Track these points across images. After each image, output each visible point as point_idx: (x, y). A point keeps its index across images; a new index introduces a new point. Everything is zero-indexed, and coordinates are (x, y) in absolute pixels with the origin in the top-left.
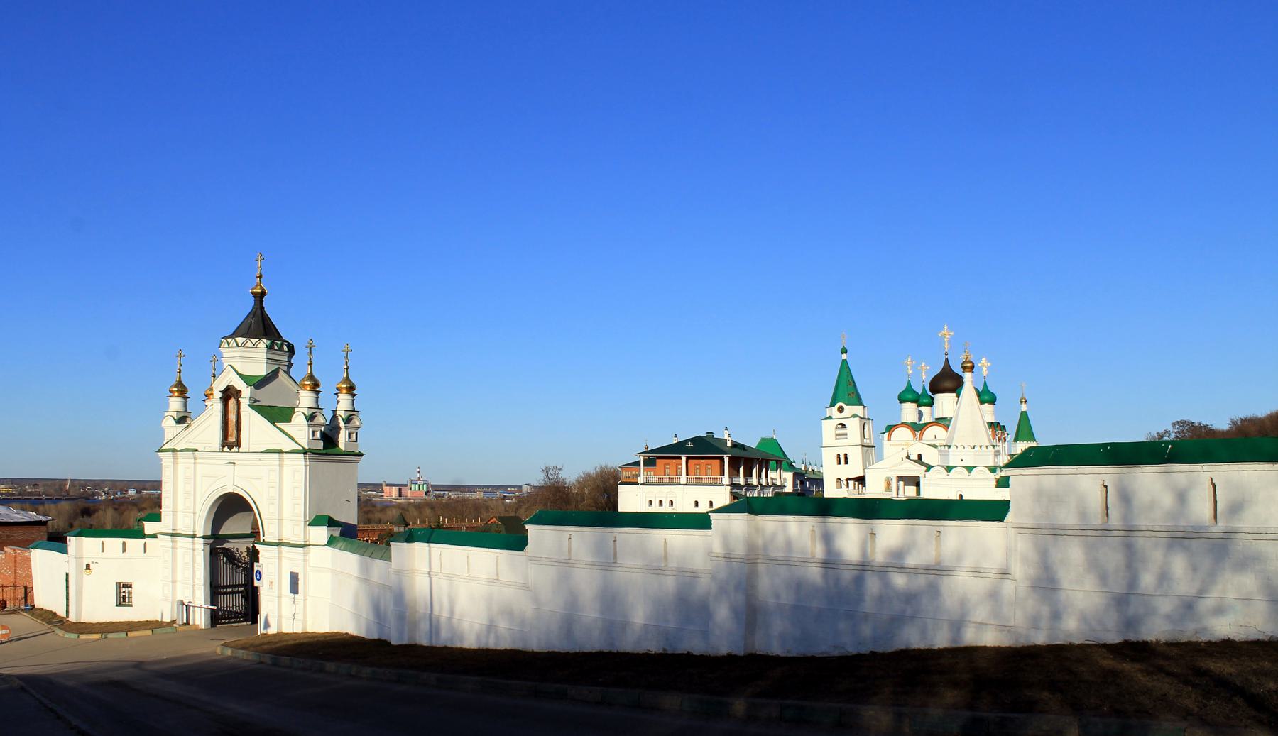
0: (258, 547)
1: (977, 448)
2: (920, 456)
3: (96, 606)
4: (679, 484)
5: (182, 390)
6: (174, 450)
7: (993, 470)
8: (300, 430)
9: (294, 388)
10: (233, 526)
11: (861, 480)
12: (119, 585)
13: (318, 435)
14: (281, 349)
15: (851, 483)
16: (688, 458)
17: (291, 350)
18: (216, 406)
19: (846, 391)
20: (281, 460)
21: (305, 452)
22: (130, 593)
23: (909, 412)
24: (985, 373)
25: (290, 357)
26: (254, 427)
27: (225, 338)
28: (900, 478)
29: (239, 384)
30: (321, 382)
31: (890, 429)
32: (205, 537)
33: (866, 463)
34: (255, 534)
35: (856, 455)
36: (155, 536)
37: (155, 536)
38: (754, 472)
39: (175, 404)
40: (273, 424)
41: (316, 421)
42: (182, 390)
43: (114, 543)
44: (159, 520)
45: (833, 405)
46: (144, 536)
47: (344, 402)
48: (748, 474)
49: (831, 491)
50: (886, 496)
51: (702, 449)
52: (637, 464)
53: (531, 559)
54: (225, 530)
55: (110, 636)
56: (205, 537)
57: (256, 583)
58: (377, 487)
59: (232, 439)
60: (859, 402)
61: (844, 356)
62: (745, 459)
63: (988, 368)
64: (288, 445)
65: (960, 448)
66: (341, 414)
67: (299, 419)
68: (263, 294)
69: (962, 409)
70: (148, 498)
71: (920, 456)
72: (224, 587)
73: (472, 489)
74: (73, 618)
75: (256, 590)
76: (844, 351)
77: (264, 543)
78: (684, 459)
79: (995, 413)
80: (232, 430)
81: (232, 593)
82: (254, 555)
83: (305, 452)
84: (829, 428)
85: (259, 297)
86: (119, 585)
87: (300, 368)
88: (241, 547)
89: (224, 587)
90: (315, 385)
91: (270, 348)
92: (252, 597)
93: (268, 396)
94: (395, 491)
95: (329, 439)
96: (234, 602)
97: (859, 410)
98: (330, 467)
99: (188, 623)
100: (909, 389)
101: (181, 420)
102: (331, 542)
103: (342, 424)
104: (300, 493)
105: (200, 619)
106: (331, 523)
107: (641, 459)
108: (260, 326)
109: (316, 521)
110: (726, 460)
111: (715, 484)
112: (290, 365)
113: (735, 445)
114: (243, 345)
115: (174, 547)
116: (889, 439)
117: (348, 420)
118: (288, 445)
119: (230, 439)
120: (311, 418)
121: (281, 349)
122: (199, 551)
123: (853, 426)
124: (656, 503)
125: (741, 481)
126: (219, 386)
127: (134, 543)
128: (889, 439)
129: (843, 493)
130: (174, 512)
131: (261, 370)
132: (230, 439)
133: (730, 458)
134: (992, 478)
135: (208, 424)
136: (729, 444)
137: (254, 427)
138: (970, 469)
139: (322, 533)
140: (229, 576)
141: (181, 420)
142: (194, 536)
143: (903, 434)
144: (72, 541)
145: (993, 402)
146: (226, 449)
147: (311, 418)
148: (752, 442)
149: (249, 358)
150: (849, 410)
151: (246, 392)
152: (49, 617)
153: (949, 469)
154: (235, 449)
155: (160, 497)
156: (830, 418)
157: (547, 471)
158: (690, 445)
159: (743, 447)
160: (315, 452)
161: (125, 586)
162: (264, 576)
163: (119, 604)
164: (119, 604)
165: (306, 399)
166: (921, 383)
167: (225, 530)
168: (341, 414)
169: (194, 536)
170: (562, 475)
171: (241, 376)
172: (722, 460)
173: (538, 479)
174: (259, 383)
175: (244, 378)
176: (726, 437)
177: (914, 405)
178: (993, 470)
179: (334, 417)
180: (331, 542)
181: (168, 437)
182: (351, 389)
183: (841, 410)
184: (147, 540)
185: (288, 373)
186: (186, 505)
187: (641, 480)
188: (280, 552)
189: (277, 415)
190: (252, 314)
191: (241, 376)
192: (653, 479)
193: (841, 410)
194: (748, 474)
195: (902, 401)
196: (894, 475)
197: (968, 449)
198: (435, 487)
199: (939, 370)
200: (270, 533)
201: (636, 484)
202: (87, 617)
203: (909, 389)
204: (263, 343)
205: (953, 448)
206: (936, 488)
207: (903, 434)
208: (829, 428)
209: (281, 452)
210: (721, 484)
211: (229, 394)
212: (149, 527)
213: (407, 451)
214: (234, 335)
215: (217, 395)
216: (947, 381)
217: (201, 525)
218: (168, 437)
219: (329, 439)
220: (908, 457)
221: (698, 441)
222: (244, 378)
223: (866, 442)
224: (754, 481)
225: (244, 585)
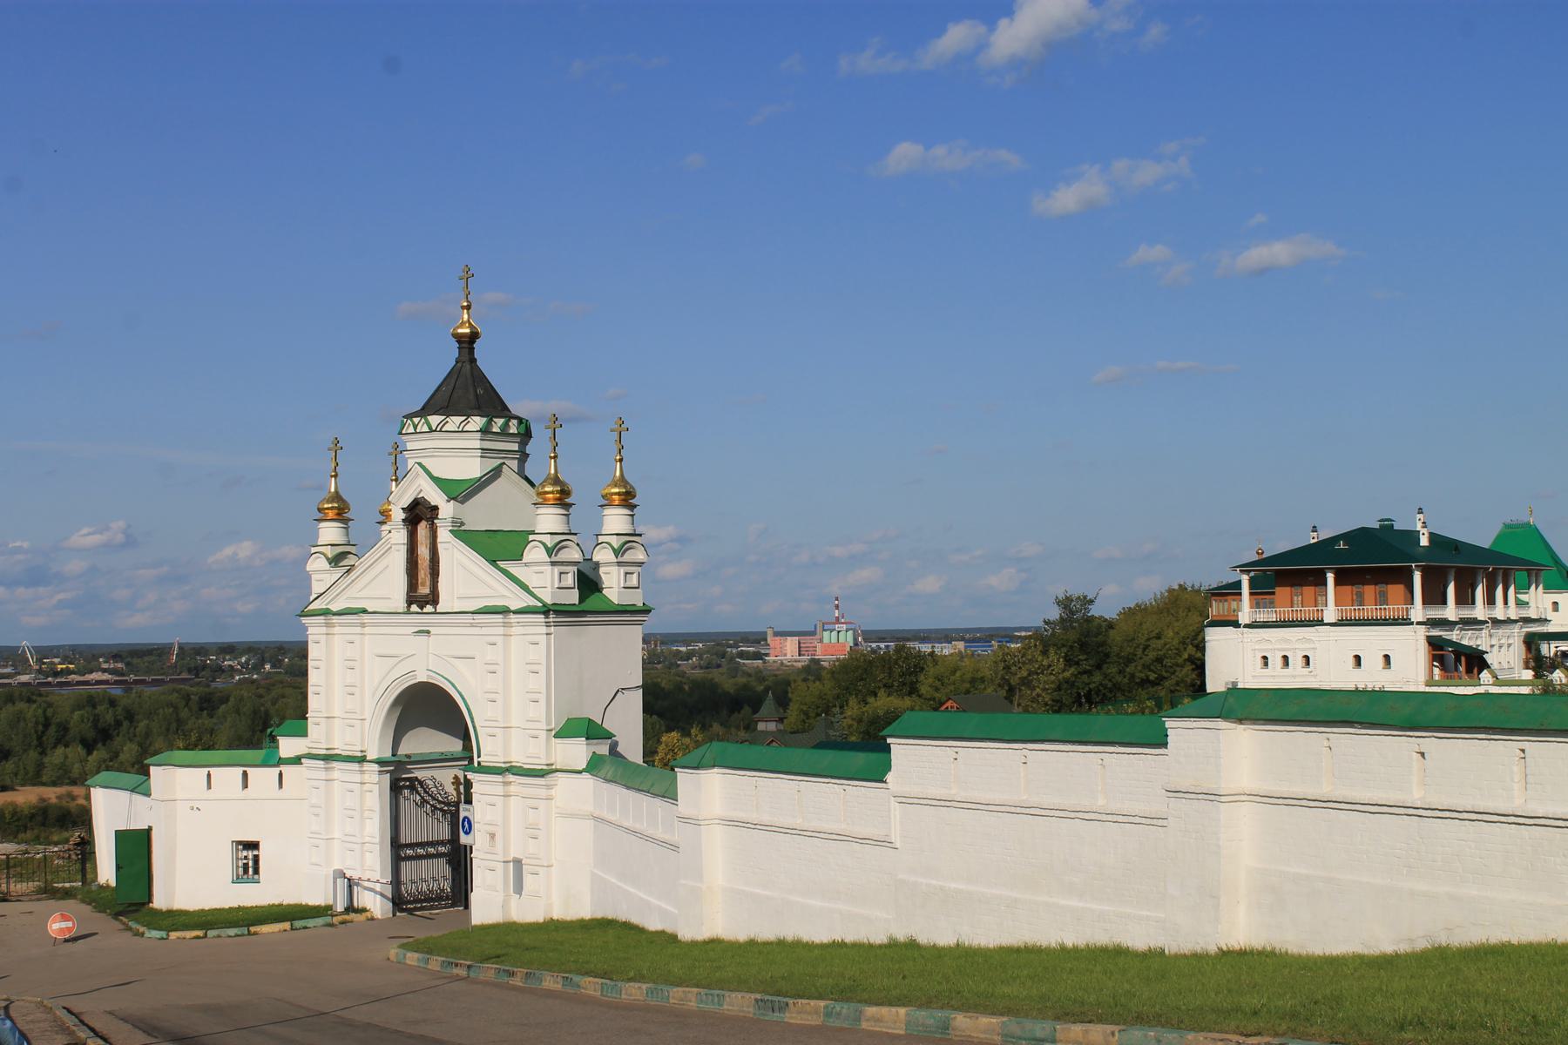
0: (470, 776)
4: (1320, 623)
6: (326, 613)
18: (397, 536)
21: (546, 611)
22: (256, 859)
25: (523, 444)
29: (435, 496)
30: (572, 485)
34: (467, 755)
36: (297, 760)
37: (297, 760)
38: (1480, 592)
40: (493, 562)
44: (147, 834)
46: (281, 762)
48: (1465, 599)
53: (905, 800)
57: (464, 839)
59: (424, 590)
67: (535, 553)
68: (474, 336)
81: (429, 856)
83: (546, 611)
85: (468, 343)
88: (445, 778)
89: (411, 846)
92: (460, 860)
93: (484, 513)
96: (431, 874)
101: (336, 561)
104: (538, 683)
105: (375, 903)
107: (1245, 579)
108: (467, 392)
109: (566, 731)
110: (1417, 577)
112: (523, 457)
118: (518, 600)
119: (422, 593)
121: (504, 433)
122: (372, 789)
124: (1275, 661)
125: (1451, 611)
126: (401, 498)
127: (263, 777)
130: (472, 625)
131: (470, 468)
132: (422, 593)
135: (383, 575)
136: (1424, 541)
139: (577, 751)
141: (336, 561)
146: (414, 608)
148: (1481, 536)
149: (452, 451)
154: (429, 608)
157: (1065, 603)
162: (476, 826)
163: (237, 880)
165: (549, 520)
167: (403, 750)
169: (362, 760)
170: (1095, 611)
171: (438, 481)
173: (1040, 612)
189: (500, 547)
191: (438, 481)
194: (1465, 599)
200: (489, 750)
201: (1236, 624)
209: (505, 611)
210: (1406, 622)
211: (419, 513)
214: (425, 411)
215: (398, 515)
217: (373, 740)
218: (317, 588)
221: (1359, 538)
224: (1479, 611)
225: (449, 841)
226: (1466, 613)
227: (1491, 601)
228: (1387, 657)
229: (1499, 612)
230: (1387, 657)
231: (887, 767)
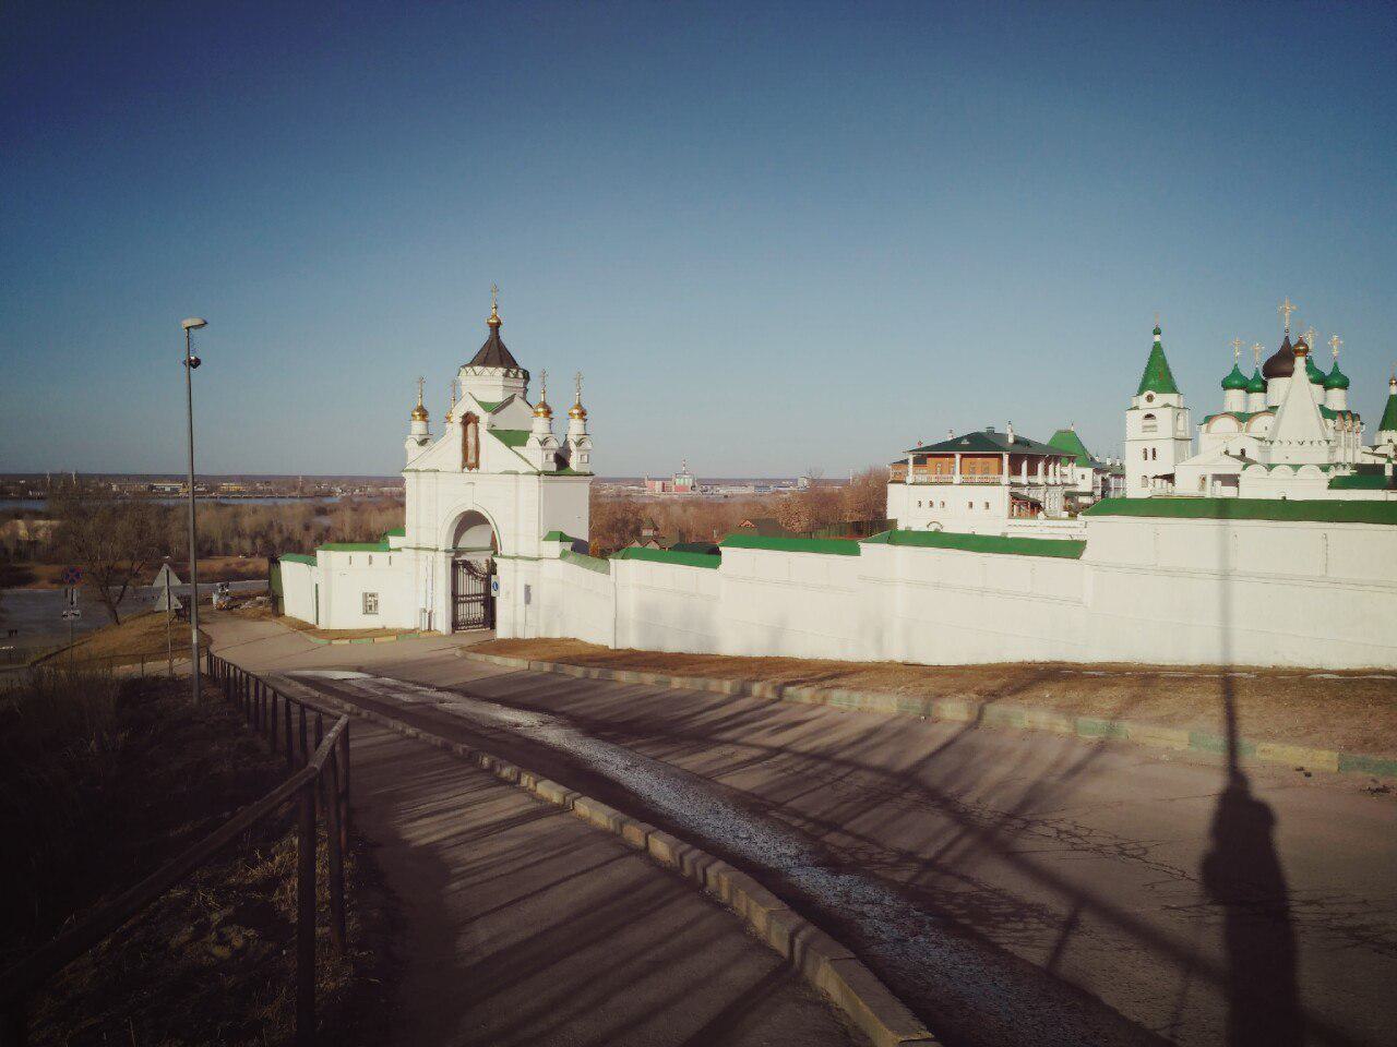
0: (496, 560)
1: (1307, 444)
2: (1243, 452)
3: (343, 614)
5: (424, 414)
6: (417, 471)
7: (1325, 468)
8: (536, 456)
9: (530, 412)
10: (474, 538)
11: (1170, 478)
12: (365, 595)
13: (552, 458)
14: (516, 376)
15: (1158, 481)
16: (963, 456)
17: (527, 376)
18: (455, 430)
19: (1158, 376)
20: (517, 481)
23: (1235, 400)
24: (1335, 353)
25: (526, 383)
26: (493, 451)
27: (464, 367)
28: (1216, 477)
29: (478, 411)
31: (1209, 419)
32: (447, 551)
33: (1179, 458)
35: (1166, 450)
36: (399, 550)
37: (399, 550)
38: (1041, 466)
39: (418, 427)
41: (548, 445)
42: (424, 414)
43: (360, 557)
45: (1141, 392)
47: (575, 427)
48: (1032, 471)
49: (1134, 488)
50: (1201, 494)
51: (981, 446)
52: (905, 462)
54: (461, 545)
55: (334, 642)
56: (447, 551)
57: (493, 593)
58: (639, 482)
59: (472, 460)
60: (1174, 390)
61: (1157, 338)
62: (1026, 455)
63: (1340, 346)
64: (523, 467)
65: (1286, 444)
66: (573, 438)
67: (533, 442)
69: (1295, 392)
70: (391, 496)
71: (1243, 452)
72: (463, 596)
73: (742, 483)
74: (322, 626)
75: (493, 600)
76: (1157, 332)
77: (501, 556)
78: (958, 457)
79: (1347, 399)
80: (471, 452)
82: (492, 569)
84: (1134, 420)
85: (495, 327)
86: (365, 595)
87: (535, 395)
88: (480, 561)
89: (463, 596)
90: (548, 412)
91: (506, 375)
92: (489, 604)
93: (505, 421)
94: (658, 485)
95: (562, 460)
96: (477, 611)
97: (1172, 398)
98: (563, 486)
99: (429, 630)
100: (1236, 373)
101: (423, 443)
102: (563, 556)
103: (573, 446)
105: (442, 624)
106: (563, 538)
107: (911, 458)
108: (495, 354)
109: (550, 537)
110: (1006, 458)
111: (993, 484)
112: (526, 390)
113: (1017, 441)
114: (480, 374)
115: (417, 560)
116: (1208, 431)
117: (579, 444)
118: (523, 467)
120: (544, 442)
122: (442, 565)
123: (1164, 418)
128: (1208, 431)
129: (1144, 493)
131: (497, 396)
132: (470, 459)
133: (1011, 457)
134: (1325, 477)
136: (1011, 440)
137: (493, 451)
138: (1296, 467)
139: (555, 548)
140: (471, 586)
142: (437, 550)
143: (1225, 425)
144: (320, 554)
145: (1344, 385)
146: (466, 470)
147: (544, 442)
149: (488, 384)
150: (1160, 399)
151: (484, 417)
152: (304, 627)
153: (1270, 467)
154: (474, 470)
155: (402, 494)
156: (1136, 408)
158: (965, 442)
159: (1027, 443)
160: (548, 474)
161: (372, 595)
163: (366, 613)
164: (366, 613)
165: (539, 426)
166: (1251, 368)
168: (573, 438)
169: (437, 550)
172: (1000, 457)
174: (494, 409)
175: (482, 404)
176: (1008, 431)
177: (1242, 392)
178: (1325, 468)
179: (566, 442)
180: (563, 556)
181: (411, 457)
182: (583, 414)
183: (1150, 398)
184: (392, 553)
185: (524, 398)
186: (430, 510)
187: (909, 479)
188: (516, 565)
189: (514, 438)
190: (488, 345)
192: (921, 478)
193: (1150, 398)
194: (1032, 471)
195: (1226, 386)
196: (1209, 473)
197: (1295, 444)
198: (702, 482)
199: (1275, 350)
200: (506, 547)
202: (335, 625)
203: (1236, 373)
204: (501, 370)
205: (1275, 444)
206: (1254, 487)
207: (1225, 425)
208: (1134, 420)
209: (517, 473)
210: (999, 484)
212: (394, 541)
213: (675, 440)
214: (472, 364)
215: (457, 418)
216: (1278, 365)
217: (443, 540)
219: (562, 460)
220: (1227, 453)
222: (482, 404)
223: (1181, 434)
224: (1040, 479)
226: (1033, 480)
227: (1046, 473)
228: (987, 504)
229: (1051, 480)
230: (987, 504)
231: (719, 562)
